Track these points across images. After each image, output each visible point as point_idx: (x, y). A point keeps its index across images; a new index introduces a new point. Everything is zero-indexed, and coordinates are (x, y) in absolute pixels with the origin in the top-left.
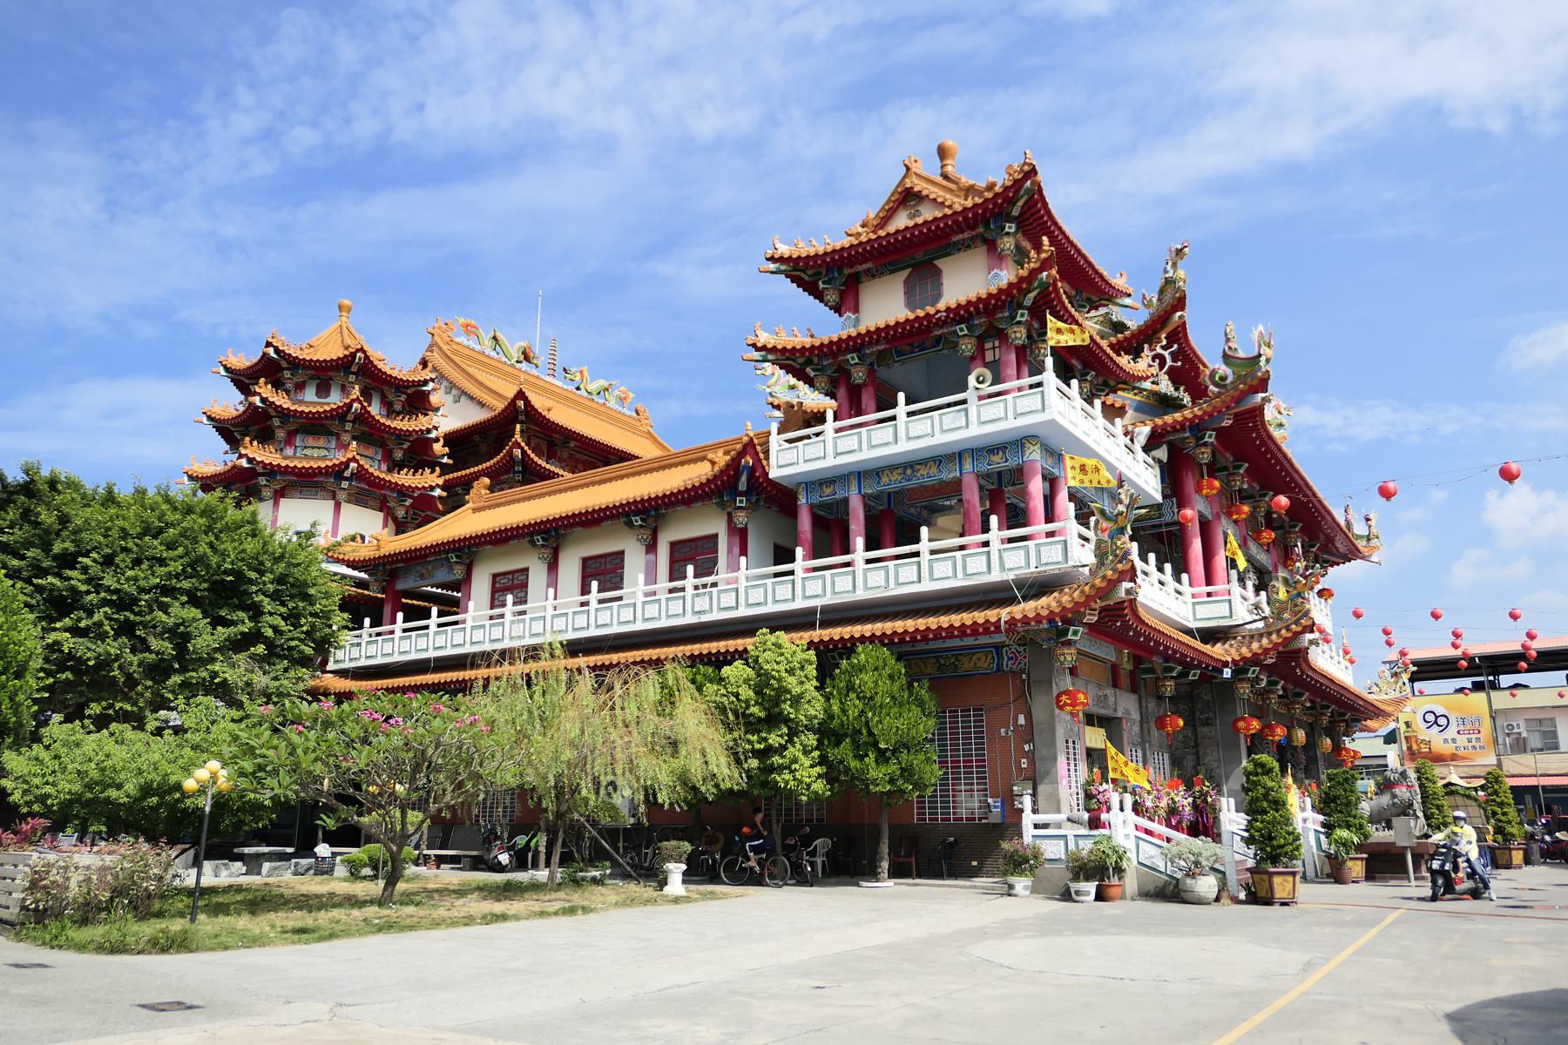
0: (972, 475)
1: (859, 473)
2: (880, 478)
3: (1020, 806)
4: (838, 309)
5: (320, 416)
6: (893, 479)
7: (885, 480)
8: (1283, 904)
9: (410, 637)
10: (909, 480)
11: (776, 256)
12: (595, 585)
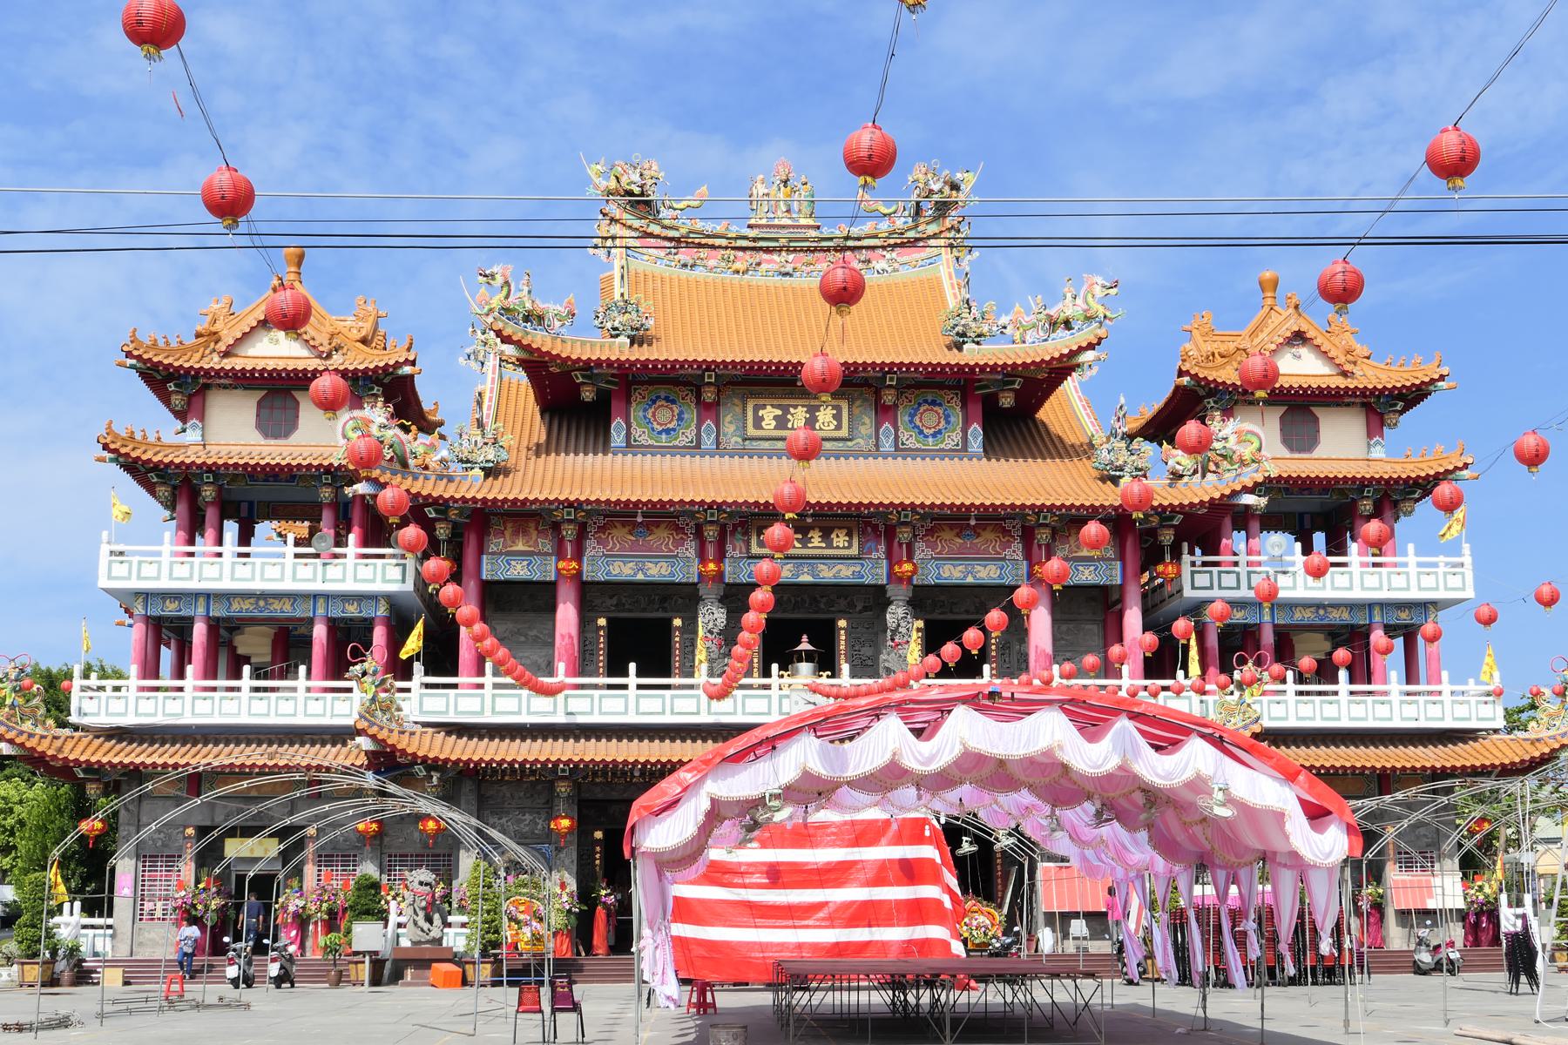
0: (1271, 625)
1: (147, 594)
2: (230, 604)
3: (385, 907)
4: (182, 415)
5: (296, 375)
6: (245, 607)
7: (235, 606)
8: (30, 986)
9: (1416, 702)
10: (261, 612)
11: (525, 342)
12: (775, 667)
